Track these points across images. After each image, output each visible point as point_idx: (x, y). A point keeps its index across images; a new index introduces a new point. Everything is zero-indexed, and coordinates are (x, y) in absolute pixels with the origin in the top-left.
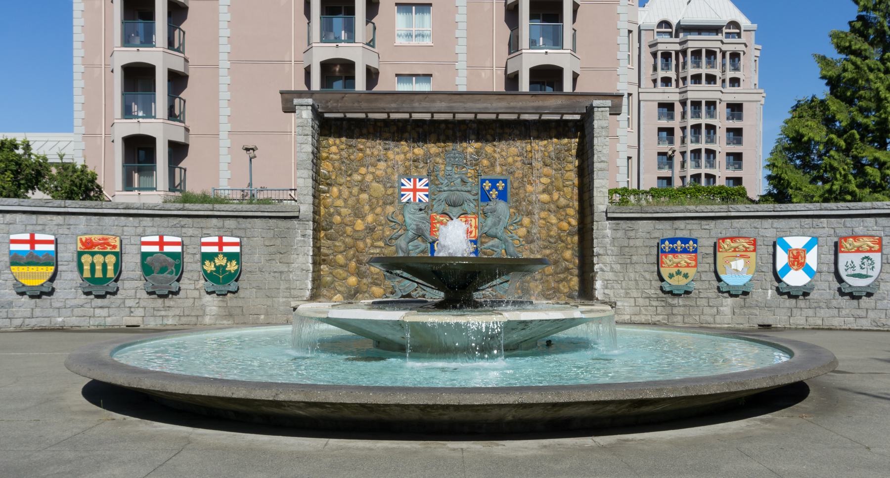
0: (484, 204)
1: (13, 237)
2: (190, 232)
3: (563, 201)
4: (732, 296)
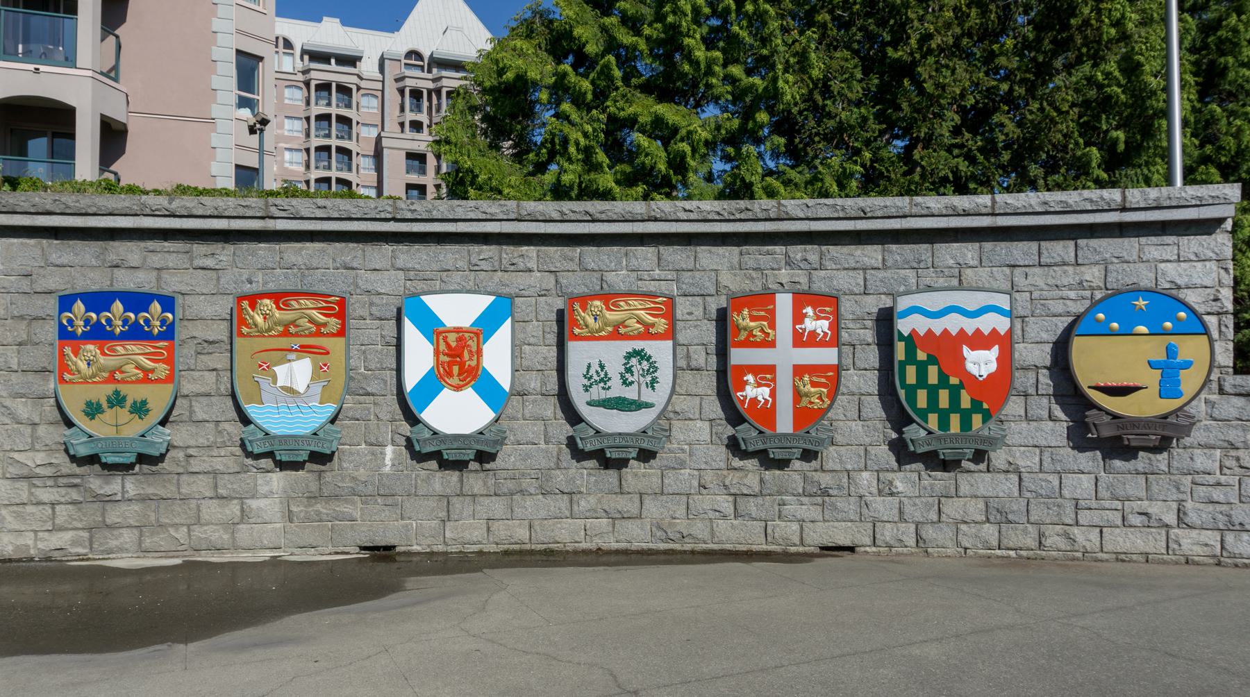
4: (282, 466)
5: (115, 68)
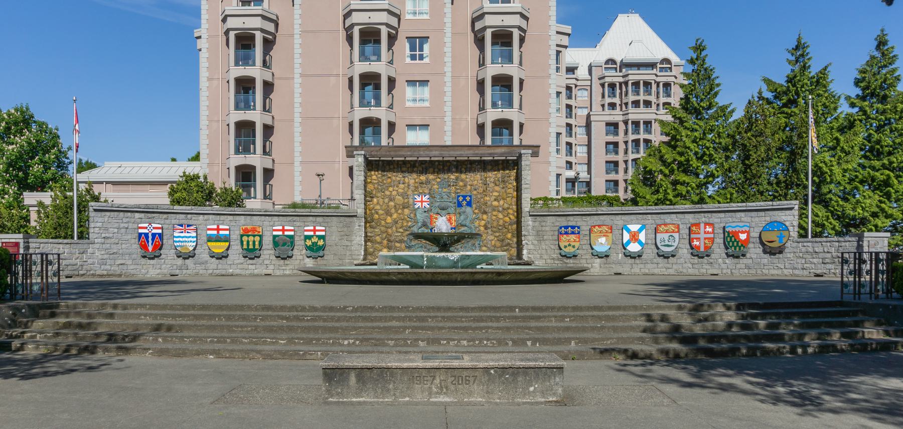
0: (459, 208)
1: (209, 227)
2: (298, 224)
3: (506, 206)
4: (599, 257)
5: (392, 60)
